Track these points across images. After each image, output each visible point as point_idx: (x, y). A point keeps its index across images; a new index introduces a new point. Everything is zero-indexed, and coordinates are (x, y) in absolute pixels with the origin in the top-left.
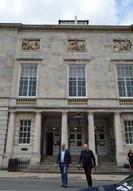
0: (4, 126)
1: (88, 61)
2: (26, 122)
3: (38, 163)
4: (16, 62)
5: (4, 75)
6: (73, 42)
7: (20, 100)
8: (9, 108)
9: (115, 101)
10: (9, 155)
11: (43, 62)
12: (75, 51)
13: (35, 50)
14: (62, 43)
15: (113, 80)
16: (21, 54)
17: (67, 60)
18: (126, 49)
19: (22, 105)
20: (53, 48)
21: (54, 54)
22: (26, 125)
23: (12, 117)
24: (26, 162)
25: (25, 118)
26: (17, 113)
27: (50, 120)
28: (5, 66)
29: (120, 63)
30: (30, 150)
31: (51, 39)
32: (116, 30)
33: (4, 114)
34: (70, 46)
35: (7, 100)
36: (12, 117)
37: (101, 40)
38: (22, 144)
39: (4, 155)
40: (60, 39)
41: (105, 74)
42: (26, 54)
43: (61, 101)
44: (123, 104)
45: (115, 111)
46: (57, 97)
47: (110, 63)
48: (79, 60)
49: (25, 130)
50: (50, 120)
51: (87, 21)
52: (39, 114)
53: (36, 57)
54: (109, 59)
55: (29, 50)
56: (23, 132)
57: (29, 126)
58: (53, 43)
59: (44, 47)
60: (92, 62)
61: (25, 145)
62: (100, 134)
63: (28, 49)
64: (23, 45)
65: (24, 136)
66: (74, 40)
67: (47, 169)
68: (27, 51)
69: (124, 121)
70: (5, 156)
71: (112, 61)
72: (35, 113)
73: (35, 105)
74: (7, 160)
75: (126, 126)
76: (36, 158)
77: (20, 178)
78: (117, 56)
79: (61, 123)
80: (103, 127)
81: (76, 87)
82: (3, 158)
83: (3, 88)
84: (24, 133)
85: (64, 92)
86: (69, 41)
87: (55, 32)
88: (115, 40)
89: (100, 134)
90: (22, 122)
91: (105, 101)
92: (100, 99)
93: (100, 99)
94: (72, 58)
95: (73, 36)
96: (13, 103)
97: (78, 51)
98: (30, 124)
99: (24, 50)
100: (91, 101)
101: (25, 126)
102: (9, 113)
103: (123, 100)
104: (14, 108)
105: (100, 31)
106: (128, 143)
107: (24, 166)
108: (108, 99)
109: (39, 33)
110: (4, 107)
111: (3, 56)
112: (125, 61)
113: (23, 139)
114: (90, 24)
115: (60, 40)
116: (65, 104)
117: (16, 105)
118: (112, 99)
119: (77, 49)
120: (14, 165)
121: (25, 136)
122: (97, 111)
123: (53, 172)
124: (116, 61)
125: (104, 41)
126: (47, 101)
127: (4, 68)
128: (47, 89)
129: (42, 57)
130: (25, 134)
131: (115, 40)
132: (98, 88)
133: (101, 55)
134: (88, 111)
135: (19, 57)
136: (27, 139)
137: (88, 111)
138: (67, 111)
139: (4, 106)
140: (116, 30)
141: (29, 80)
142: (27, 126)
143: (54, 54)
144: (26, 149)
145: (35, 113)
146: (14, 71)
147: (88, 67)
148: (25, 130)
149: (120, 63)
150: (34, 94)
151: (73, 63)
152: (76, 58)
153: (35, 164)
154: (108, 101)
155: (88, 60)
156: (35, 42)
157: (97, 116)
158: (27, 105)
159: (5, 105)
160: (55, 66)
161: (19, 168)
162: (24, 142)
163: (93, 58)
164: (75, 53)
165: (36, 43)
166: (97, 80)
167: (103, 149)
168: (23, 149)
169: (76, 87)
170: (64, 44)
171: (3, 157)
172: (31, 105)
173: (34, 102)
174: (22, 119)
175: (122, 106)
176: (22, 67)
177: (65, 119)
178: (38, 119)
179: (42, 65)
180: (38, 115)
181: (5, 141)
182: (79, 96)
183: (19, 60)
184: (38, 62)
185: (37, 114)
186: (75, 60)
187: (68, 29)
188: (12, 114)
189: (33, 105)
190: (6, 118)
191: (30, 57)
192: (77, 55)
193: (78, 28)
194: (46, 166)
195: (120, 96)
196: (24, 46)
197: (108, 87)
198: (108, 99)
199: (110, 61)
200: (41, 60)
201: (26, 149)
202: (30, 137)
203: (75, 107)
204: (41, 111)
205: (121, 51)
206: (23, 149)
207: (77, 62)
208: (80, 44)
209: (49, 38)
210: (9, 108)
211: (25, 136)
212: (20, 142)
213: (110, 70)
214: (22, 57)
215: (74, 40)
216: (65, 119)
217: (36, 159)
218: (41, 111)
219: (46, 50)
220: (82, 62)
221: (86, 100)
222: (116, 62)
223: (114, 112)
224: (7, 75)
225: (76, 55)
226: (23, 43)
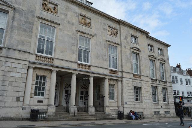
0: (24, 79)
1: (92, 36)
2: (41, 77)
3: (54, 113)
4: (36, 19)
5: (25, 29)
6: (83, 18)
7: (39, 57)
8: (30, 62)
9: (106, 70)
10: (28, 106)
11: (60, 27)
12: (85, 25)
13: (54, 13)
14: (75, 16)
15: (106, 55)
16: (41, 13)
17: (79, 31)
18: (114, 34)
19: (41, 62)
20: (68, 16)
21: (69, 22)
22: (41, 79)
23: (31, 71)
24: (44, 113)
25: (42, 73)
26: (35, 68)
27: (63, 78)
28: (26, 20)
29: (111, 43)
30: (45, 102)
31: (67, 9)
32: (85, 7)
33: (25, 68)
34: (81, 20)
35: (27, 54)
36: (31, 71)
37: (101, 23)
38: (37, 97)
39: (23, 106)
40: (74, 11)
41: (102, 49)
42: (46, 14)
43: (73, 63)
44: (87, 69)
45: (106, 77)
46: (70, 60)
47: (105, 42)
48: (87, 34)
49: (40, 84)
50: (63, 78)
51: (92, 4)
52: (32, 68)
53: (54, 21)
54: (105, 38)
55: (48, 12)
56: (38, 86)
57: (44, 81)
58: (69, 13)
59: (61, 13)
60: (95, 38)
61: (40, 98)
62: (81, 91)
63: (48, 10)
64: (43, 5)
65: (39, 90)
66: (84, 16)
67: (63, 118)
68: (46, 11)
69: (37, 76)
70: (24, 108)
71: (107, 41)
72: (51, 71)
73: (53, 64)
74: (28, 111)
75: (37, 81)
76: (53, 109)
77: (59, 125)
78: (110, 38)
79: (70, 81)
80: (81, 85)
81: (83, 55)
82: (23, 110)
83: (23, 42)
84: (39, 87)
85: (74, 57)
86: (80, 15)
87: (71, 4)
88: (109, 26)
89: (81, 91)
90: (38, 76)
91: (101, 69)
92: (98, 67)
93: (98, 67)
94: (82, 30)
95: (84, 13)
96: (33, 59)
97: (86, 26)
98: (44, 80)
99: (43, 10)
100: (58, 60)
101: (41, 81)
102: (29, 68)
103: (42, 57)
104: (34, 63)
105: (91, 11)
106: (36, 96)
107: (42, 116)
108: (103, 68)
109: (114, 24)
110: (14, 59)
111: (24, 9)
112: (114, 43)
113: (37, 92)
114: (92, 6)
115: (74, 12)
116: (75, 66)
117: (36, 61)
118: (105, 68)
119: (85, 24)
120: (35, 115)
121: (39, 90)
122: (96, 75)
123: (92, 119)
124: (109, 41)
125: (103, 24)
126: (62, 61)
127: (25, 22)
128: (62, 52)
129: (59, 22)
130: (40, 88)
131: (109, 26)
132: (98, 58)
133: (100, 35)
134: (91, 74)
135: (39, 15)
136: (40, 90)
137: (91, 74)
138: (77, 72)
139: (25, 59)
140: (85, 7)
141: (46, 39)
142: (42, 81)
143: (69, 22)
144: (41, 102)
145: (51, 71)
146: (34, 28)
147: (93, 41)
148: (40, 84)
149: (111, 43)
150: (51, 54)
151: (82, 34)
152: (85, 31)
153: (51, 114)
154: (103, 69)
155: (93, 36)
156: (54, 6)
157: (95, 79)
158: (45, 62)
159: (26, 59)
160: (70, 34)
161: (39, 118)
162: (39, 95)
163: (96, 35)
164: (84, 27)
165: (55, 8)
166: (97, 53)
167: (139, 103)
168: (39, 102)
169: (83, 55)
170: (77, 16)
171: (23, 108)
172: (50, 63)
173: (51, 61)
174: (39, 74)
175: (110, 74)
176: (41, 25)
177: (74, 78)
178: (54, 75)
179: (60, 29)
180: (54, 73)
181: (24, 93)
182: (112, 68)
183: (39, 18)
184: (56, 26)
185: (54, 72)
186: (84, 33)
187: (87, 8)
188: (31, 68)
189: (51, 64)
190: (26, 71)
191: (49, 19)
192: (85, 29)
193: (88, 8)
194: (61, 116)
195: (38, 52)
196: (44, 7)
197: (103, 59)
198: (103, 68)
199: (105, 41)
200: (59, 24)
201: (41, 102)
202: (35, 92)
203: (83, 71)
204: (58, 69)
205: (111, 35)
206: (39, 102)
207: (85, 35)
208: (88, 21)
209: (65, 7)
210: (29, 63)
211: (39, 90)
212: (35, 95)
213: (105, 47)
214: (42, 16)
215: (84, 16)
216: (74, 78)
217: (52, 111)
218: (58, 69)
219: (63, 17)
220: (88, 36)
221: (90, 66)
222: (108, 42)
223: (106, 78)
224: (27, 30)
225: (84, 29)
226: (44, 3)
